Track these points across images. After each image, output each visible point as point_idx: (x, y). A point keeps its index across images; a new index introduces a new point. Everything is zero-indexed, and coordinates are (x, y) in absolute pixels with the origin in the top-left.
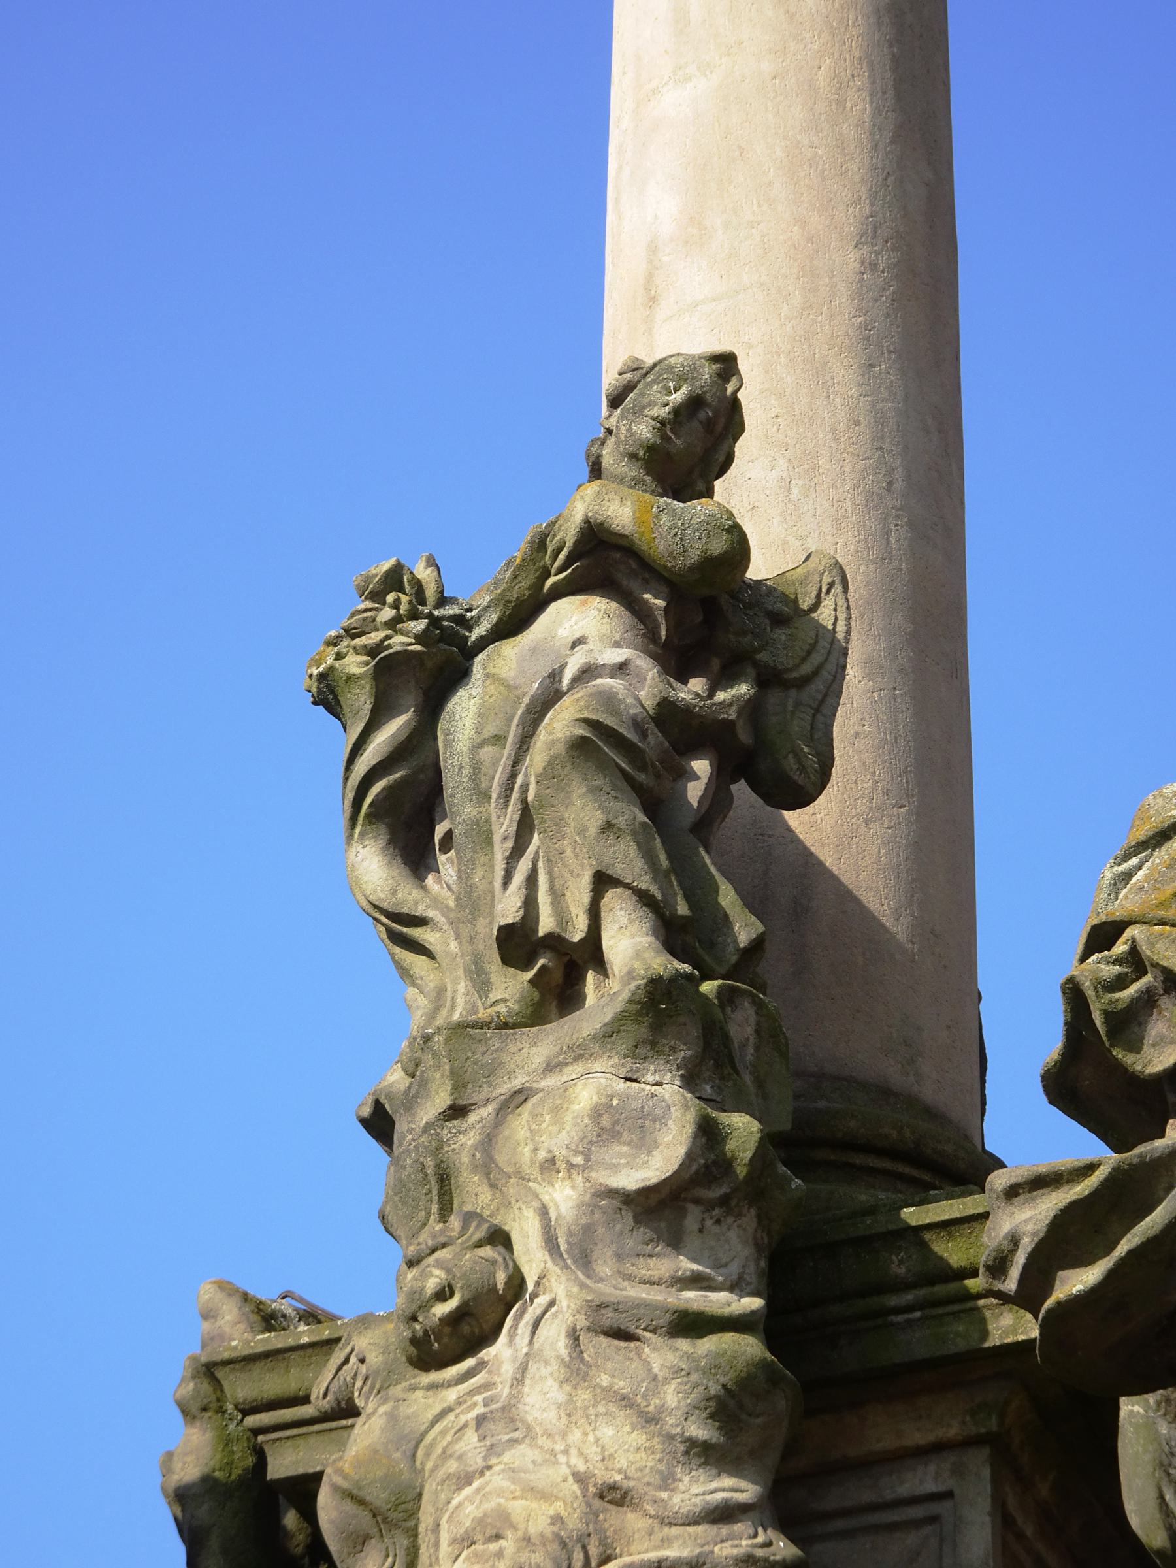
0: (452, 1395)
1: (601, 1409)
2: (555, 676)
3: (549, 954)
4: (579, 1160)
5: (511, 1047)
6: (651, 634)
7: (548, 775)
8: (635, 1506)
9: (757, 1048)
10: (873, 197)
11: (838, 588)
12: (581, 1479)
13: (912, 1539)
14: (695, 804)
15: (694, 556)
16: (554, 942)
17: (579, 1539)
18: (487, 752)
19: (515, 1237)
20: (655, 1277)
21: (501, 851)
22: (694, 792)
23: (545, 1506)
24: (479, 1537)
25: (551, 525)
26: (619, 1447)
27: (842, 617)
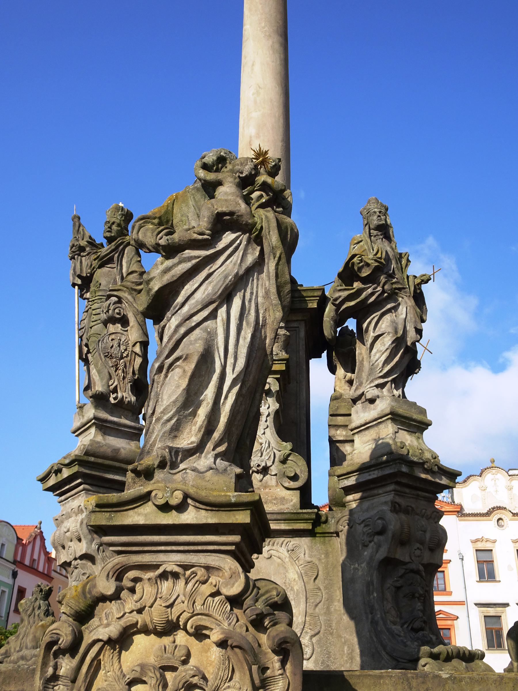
15: (280, 189)
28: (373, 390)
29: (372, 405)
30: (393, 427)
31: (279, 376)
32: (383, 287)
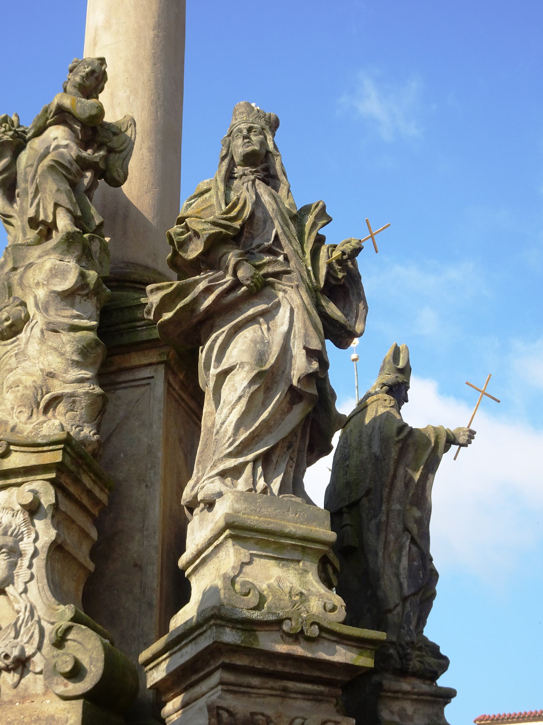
0: (9, 347)
1: (49, 351)
2: (48, 148)
3: (42, 226)
4: (46, 283)
5: (30, 251)
6: (77, 137)
7: (43, 175)
8: (57, 378)
9: (100, 253)
10: (159, 16)
11: (133, 126)
12: (42, 370)
13: (143, 389)
14: (86, 184)
15: (87, 115)
16: (44, 222)
17: (40, 387)
18: (29, 169)
19: (28, 304)
20: (66, 315)
21: (30, 196)
22: (86, 181)
23: (31, 378)
24: (13, 386)
25: (49, 105)
26: (54, 362)
27: (133, 133)
28: (213, 482)
29: (211, 513)
30: (237, 553)
31: (53, 475)
32: (235, 274)
